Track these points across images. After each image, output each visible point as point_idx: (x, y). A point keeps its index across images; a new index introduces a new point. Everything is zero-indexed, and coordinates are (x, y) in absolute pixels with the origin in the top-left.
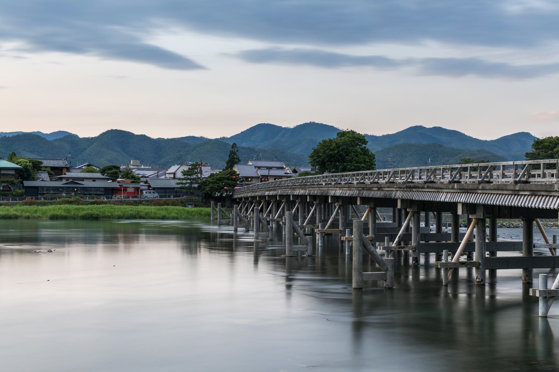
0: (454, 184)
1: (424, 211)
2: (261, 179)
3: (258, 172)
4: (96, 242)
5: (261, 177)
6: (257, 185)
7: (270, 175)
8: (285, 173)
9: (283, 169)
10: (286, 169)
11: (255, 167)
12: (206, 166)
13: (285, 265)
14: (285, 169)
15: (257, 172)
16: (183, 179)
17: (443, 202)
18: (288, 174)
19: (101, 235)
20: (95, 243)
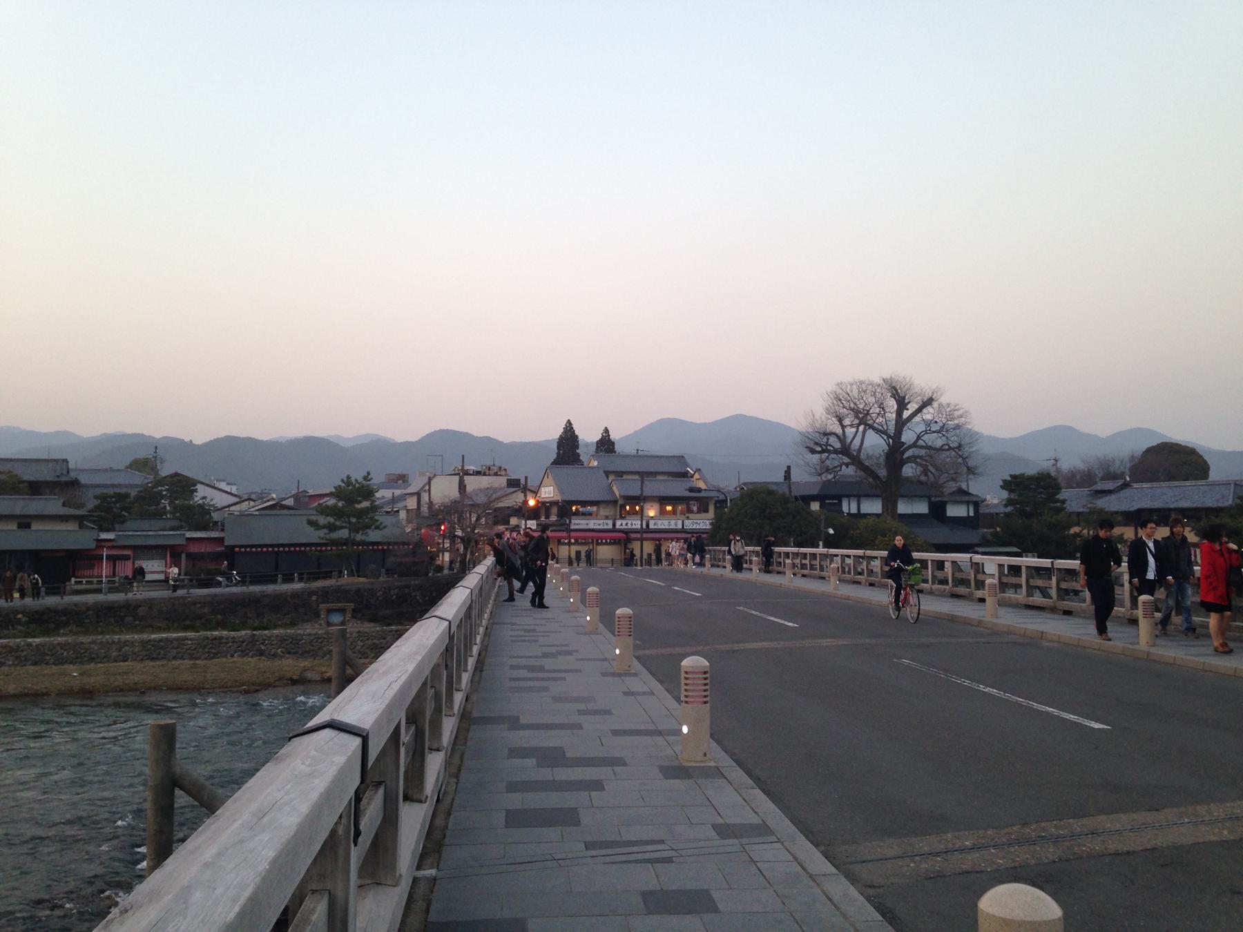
0: (1199, 566)
1: (568, 758)
2: (623, 507)
3: (615, 488)
4: (73, 607)
5: (620, 502)
6: (202, 657)
7: (644, 495)
8: (691, 490)
9: (687, 477)
10: (694, 479)
11: (607, 473)
12: (501, 475)
13: (507, 557)
14: (692, 477)
15: (611, 488)
16: (538, 636)
17: (1114, 598)
18: (699, 490)
19: (1133, 524)
20: (1195, 450)
